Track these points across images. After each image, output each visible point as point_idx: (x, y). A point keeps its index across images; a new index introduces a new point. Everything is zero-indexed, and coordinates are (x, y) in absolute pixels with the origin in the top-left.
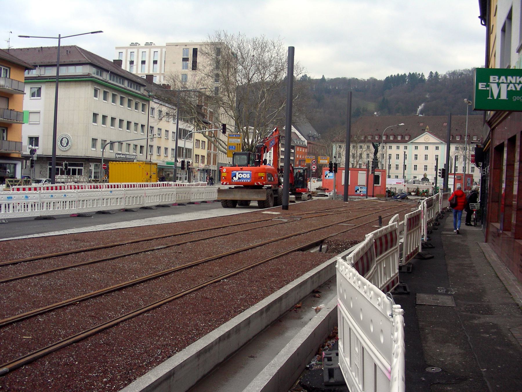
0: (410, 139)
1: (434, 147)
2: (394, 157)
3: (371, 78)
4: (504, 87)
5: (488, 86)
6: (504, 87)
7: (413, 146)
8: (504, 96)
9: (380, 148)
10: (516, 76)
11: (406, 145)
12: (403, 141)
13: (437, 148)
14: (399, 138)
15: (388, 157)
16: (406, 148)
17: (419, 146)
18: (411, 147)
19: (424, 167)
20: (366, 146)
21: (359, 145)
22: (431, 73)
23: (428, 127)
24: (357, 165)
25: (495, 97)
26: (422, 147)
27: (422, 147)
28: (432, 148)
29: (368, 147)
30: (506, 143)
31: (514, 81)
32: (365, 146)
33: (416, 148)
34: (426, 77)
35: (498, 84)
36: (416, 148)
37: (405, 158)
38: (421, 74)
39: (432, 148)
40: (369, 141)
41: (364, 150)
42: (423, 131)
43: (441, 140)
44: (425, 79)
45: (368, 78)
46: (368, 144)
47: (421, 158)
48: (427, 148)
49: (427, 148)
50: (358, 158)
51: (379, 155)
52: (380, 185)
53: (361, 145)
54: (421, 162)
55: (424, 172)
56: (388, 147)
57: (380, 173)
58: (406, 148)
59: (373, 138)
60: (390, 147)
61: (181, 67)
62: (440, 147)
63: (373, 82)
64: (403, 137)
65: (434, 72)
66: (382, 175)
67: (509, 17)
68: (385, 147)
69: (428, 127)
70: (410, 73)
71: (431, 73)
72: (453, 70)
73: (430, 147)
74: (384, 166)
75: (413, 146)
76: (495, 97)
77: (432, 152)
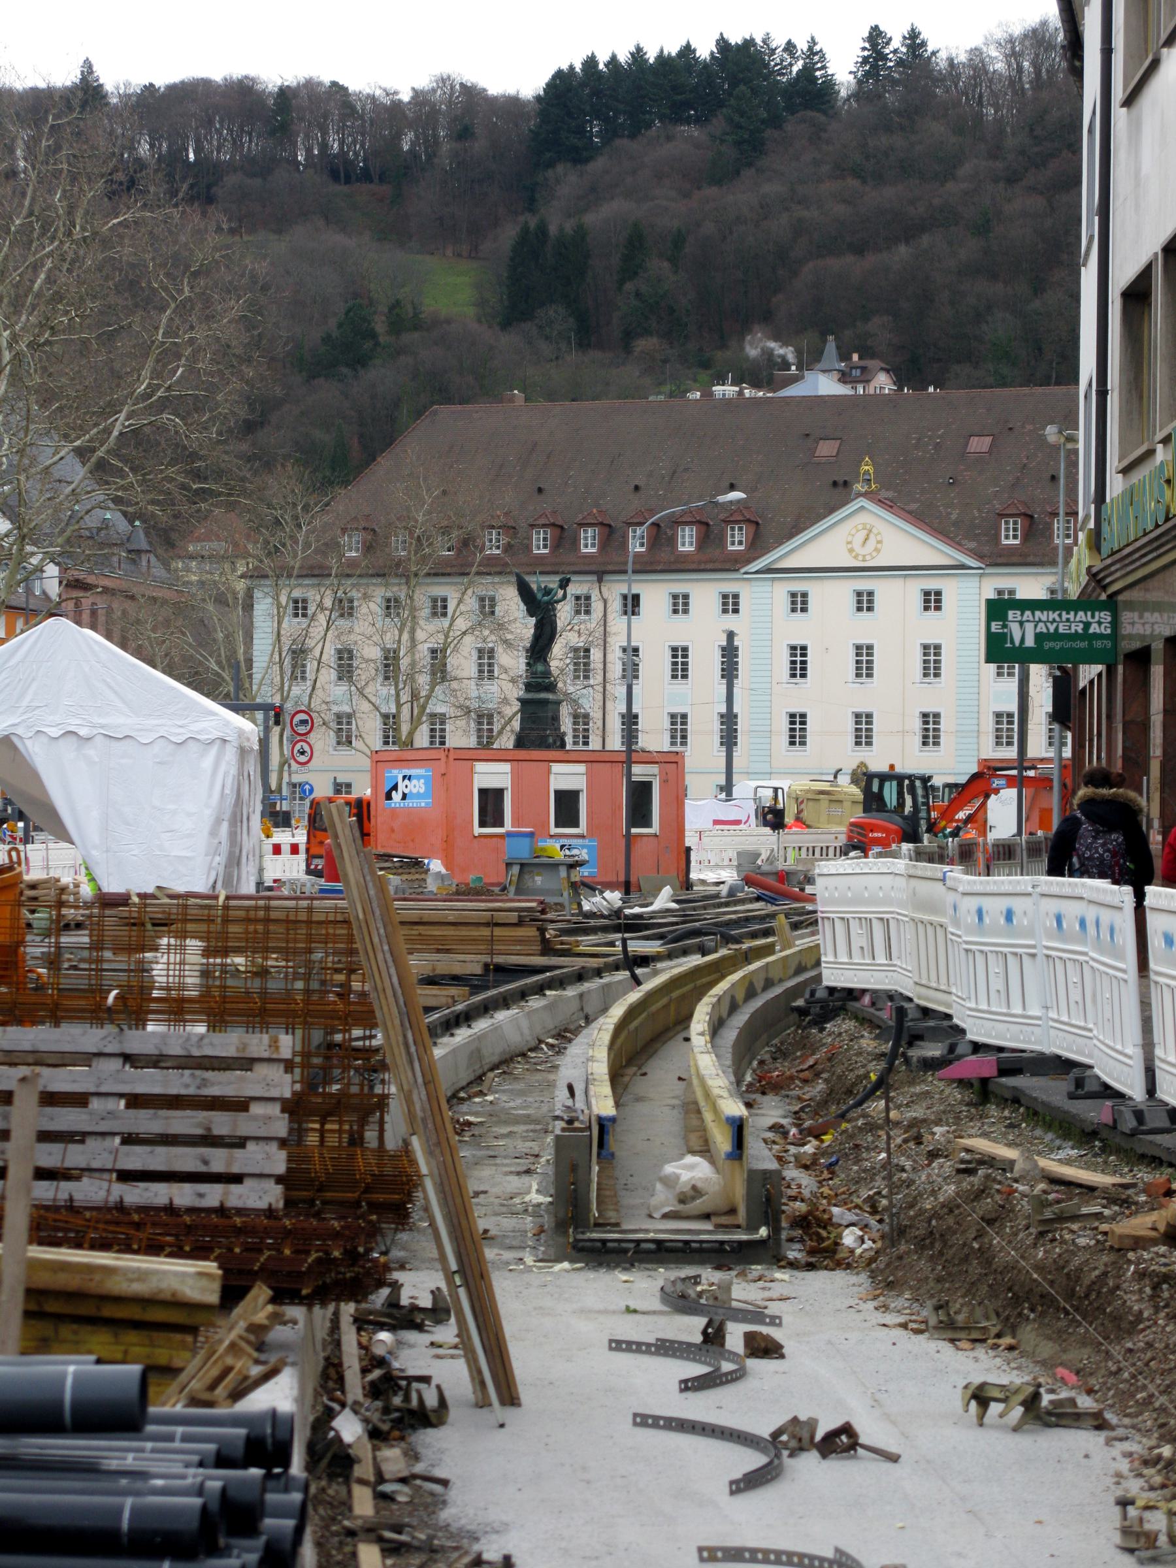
0: (758, 545)
1: (913, 590)
2: (655, 664)
3: (444, 80)
4: (1029, 627)
5: (1004, 626)
6: (1029, 627)
8: (1030, 642)
9: (564, 613)
10: (1048, 609)
11: (730, 588)
12: (713, 559)
13: (932, 601)
14: (686, 541)
15: (616, 669)
16: (731, 604)
17: (817, 591)
18: (763, 598)
19: (850, 725)
20: (471, 603)
21: (423, 595)
22: (876, 37)
23: (867, 467)
24: (415, 722)
25: (1017, 643)
26: (833, 598)
27: (833, 598)
28: (898, 597)
29: (488, 607)
30: (1158, 646)
31: (1044, 618)
32: (463, 600)
33: (799, 603)
34: (843, 67)
35: (1021, 623)
36: (799, 603)
37: (729, 671)
38: (802, 45)
39: (898, 597)
40: (493, 568)
41: (461, 624)
42: (838, 491)
44: (829, 84)
45: (424, 82)
46: (484, 586)
47: (831, 664)
48: (865, 602)
49: (865, 602)
50: (423, 680)
51: (558, 656)
52: (655, 828)
53: (439, 591)
54: (830, 696)
56: (616, 605)
57: (654, 769)
58: (731, 604)
59: (517, 547)
60: (632, 604)
61: (990, 739)
62: (953, 590)
63: (461, 114)
66: (664, 782)
67: (1090, 385)
68: (597, 606)
69: (867, 467)
71: (876, 37)
73: (886, 591)
74: (595, 726)
75: (780, 592)
76: (1017, 643)
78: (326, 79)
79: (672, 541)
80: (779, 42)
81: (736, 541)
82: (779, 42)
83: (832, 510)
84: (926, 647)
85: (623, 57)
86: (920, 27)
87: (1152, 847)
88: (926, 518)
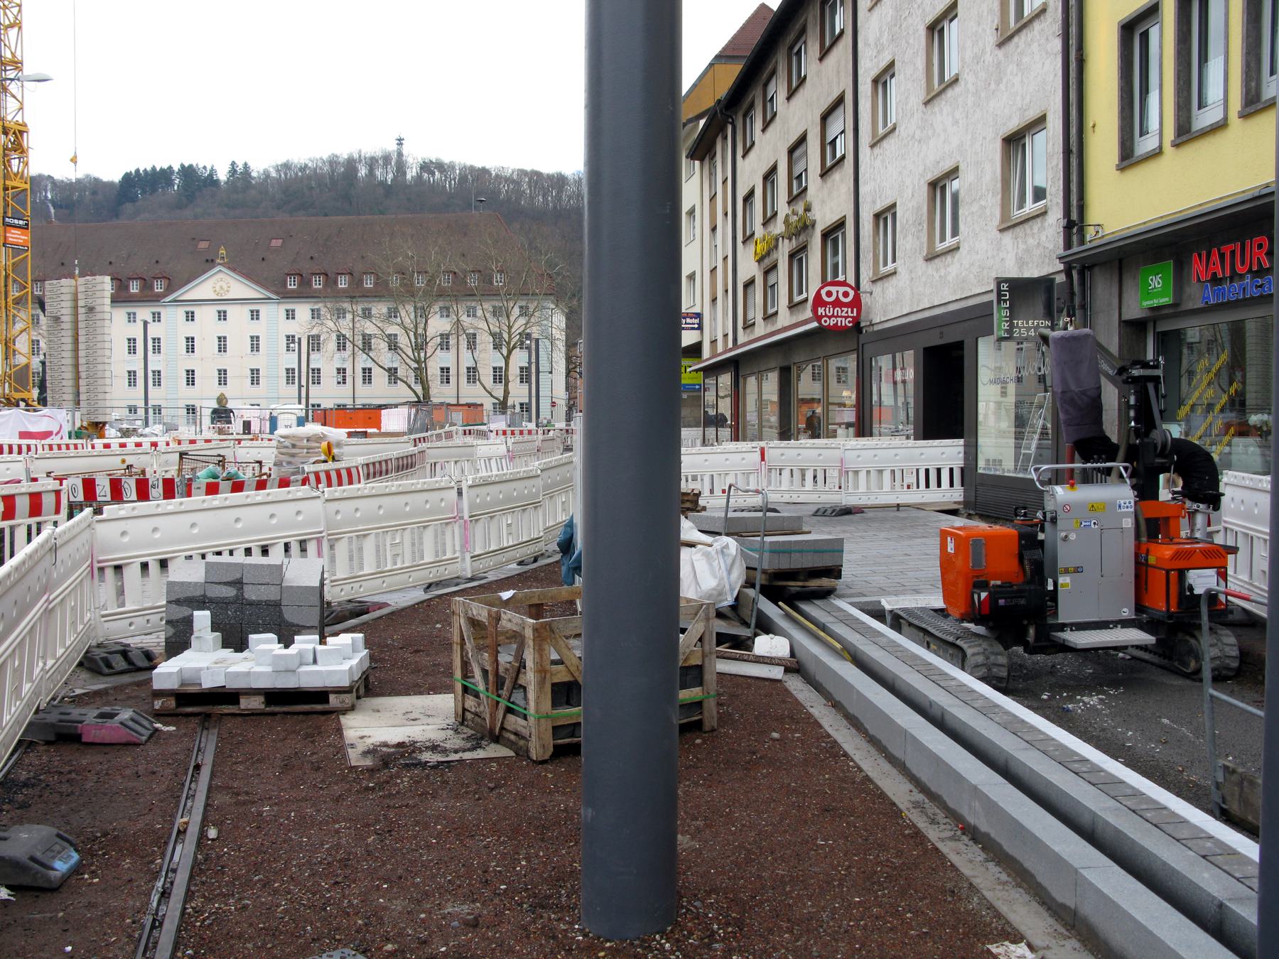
0: (170, 289)
1: (245, 310)
3: (87, 176)
7: (180, 312)
12: (148, 297)
13: (255, 315)
14: (134, 288)
17: (199, 311)
18: (173, 316)
22: (233, 164)
23: (222, 251)
26: (206, 315)
27: (206, 315)
28: (238, 314)
33: (190, 316)
34: (222, 175)
36: (190, 316)
38: (209, 168)
39: (238, 314)
42: (211, 263)
43: (267, 288)
44: (217, 182)
47: (206, 346)
48: (222, 316)
49: (222, 316)
55: (217, 390)
62: (264, 310)
64: (146, 285)
65: (240, 168)
69: (222, 251)
70: (182, 166)
71: (233, 164)
72: (283, 160)
73: (232, 310)
75: (180, 312)
77: (239, 324)
78: (46, 174)
79: (127, 288)
80: (201, 166)
81: (158, 288)
82: (201, 166)
83: (205, 272)
84: (287, 370)
85: (149, 169)
86: (250, 164)
87: (912, 371)
88: (250, 275)
